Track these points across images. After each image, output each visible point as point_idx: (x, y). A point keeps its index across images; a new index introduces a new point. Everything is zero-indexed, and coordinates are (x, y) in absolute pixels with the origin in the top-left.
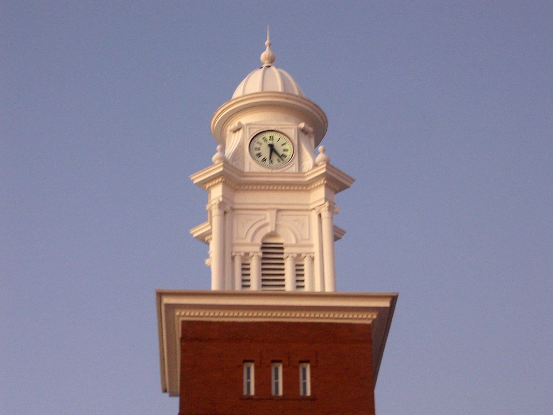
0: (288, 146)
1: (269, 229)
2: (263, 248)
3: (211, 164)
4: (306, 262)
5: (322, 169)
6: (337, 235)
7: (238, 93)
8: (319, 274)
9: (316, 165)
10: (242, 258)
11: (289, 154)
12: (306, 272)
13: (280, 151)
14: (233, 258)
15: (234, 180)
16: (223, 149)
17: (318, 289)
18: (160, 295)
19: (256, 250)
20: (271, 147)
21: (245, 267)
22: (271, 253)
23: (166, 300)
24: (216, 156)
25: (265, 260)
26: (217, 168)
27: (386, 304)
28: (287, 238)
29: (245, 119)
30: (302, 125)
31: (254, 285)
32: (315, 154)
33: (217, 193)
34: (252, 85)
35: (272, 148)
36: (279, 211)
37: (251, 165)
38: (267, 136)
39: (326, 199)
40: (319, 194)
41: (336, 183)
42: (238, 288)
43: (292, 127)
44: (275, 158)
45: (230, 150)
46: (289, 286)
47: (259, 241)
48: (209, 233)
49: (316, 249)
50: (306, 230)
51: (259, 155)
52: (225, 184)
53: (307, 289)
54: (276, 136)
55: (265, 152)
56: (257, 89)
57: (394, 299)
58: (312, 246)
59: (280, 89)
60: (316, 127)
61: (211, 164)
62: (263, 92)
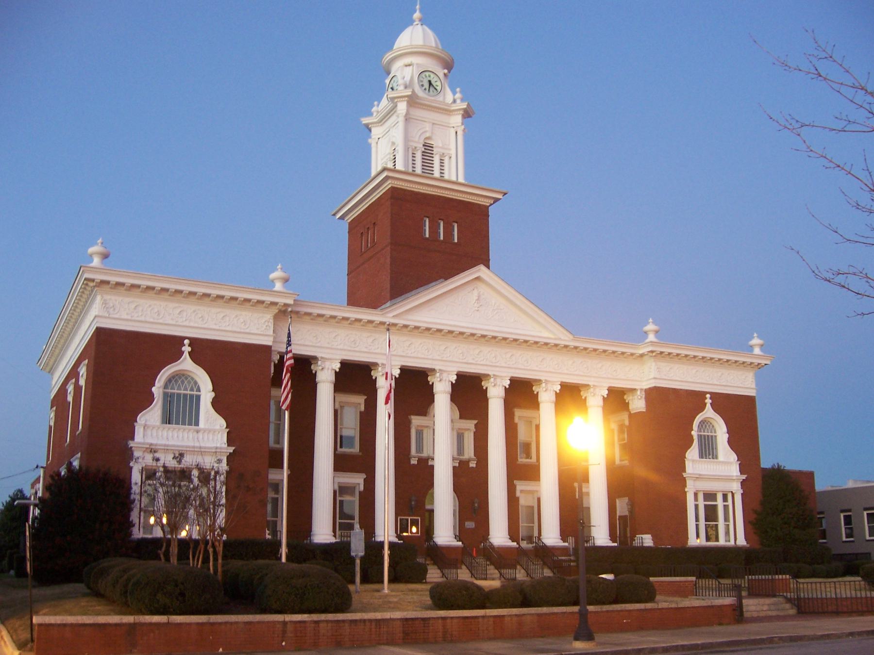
0: (439, 83)
1: (428, 135)
3: (371, 114)
4: (446, 160)
8: (452, 172)
10: (413, 150)
11: (439, 88)
13: (434, 84)
17: (454, 179)
20: (430, 81)
22: (428, 149)
28: (436, 143)
31: (419, 170)
32: (454, 93)
36: (434, 124)
37: (420, 93)
38: (427, 74)
40: (457, 120)
42: (410, 170)
46: (437, 174)
47: (422, 142)
49: (453, 152)
51: (422, 85)
52: (408, 102)
54: (432, 75)
55: (426, 85)
56: (408, 43)
58: (450, 149)
59: (434, 45)
62: (424, 46)
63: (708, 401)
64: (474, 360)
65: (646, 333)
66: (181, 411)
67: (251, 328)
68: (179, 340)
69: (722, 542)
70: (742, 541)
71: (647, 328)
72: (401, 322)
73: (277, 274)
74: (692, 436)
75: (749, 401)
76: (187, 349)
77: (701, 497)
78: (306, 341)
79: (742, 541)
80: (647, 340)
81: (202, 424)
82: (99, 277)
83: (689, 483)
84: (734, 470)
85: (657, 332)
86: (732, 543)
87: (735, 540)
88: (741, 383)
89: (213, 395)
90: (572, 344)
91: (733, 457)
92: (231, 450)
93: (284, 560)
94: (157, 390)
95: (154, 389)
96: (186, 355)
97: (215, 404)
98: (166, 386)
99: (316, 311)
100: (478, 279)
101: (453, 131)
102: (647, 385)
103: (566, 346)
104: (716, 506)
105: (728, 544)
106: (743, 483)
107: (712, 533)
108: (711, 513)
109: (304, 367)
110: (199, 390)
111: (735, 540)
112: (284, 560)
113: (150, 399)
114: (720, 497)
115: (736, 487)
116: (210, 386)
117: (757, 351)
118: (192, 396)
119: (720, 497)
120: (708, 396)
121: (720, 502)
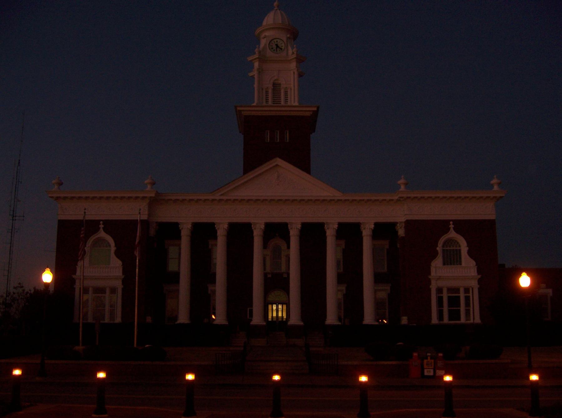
0: (283, 45)
2: (273, 85)
3: (255, 53)
4: (289, 91)
5: (295, 56)
6: (300, 75)
7: (264, 23)
8: (292, 101)
9: (293, 53)
11: (283, 48)
12: (289, 94)
14: (263, 89)
15: (263, 59)
16: (259, 47)
18: (236, 107)
19: (271, 86)
21: (267, 92)
22: (276, 86)
23: (238, 109)
24: (257, 49)
25: (274, 90)
26: (256, 56)
27: (315, 109)
29: (267, 34)
30: (288, 36)
31: (270, 103)
32: (293, 48)
33: (256, 64)
34: (269, 19)
35: (277, 45)
38: (275, 40)
39: (296, 67)
40: (293, 65)
41: (300, 60)
42: (264, 104)
43: (283, 36)
44: (278, 49)
45: (262, 46)
46: (283, 103)
48: (254, 75)
49: (292, 86)
50: (289, 78)
53: (289, 104)
54: (279, 41)
55: (275, 47)
57: (318, 108)
60: (294, 35)
61: (255, 53)
63: (452, 226)
64: (277, 215)
65: (399, 185)
66: (452, 258)
67: (133, 211)
68: (447, 222)
69: (463, 320)
70: (478, 320)
71: (492, 182)
72: (224, 198)
73: (401, 181)
74: (437, 251)
75: (492, 223)
76: (102, 226)
77: (445, 291)
78: (167, 214)
79: (478, 320)
80: (401, 190)
81: (463, 264)
82: (405, 196)
83: (433, 282)
84: (473, 272)
85: (499, 184)
86: (472, 321)
87: (474, 319)
88: (483, 211)
89: (467, 248)
90: (343, 198)
91: (473, 263)
92: (479, 277)
93: (135, 346)
94: (439, 249)
95: (438, 249)
96: (452, 229)
97: (469, 253)
98: (443, 246)
99: (174, 198)
100: (277, 165)
101: (292, 72)
102: (403, 219)
103: (338, 200)
104: (459, 297)
105: (469, 322)
106: (479, 281)
107: (454, 315)
108: (454, 302)
109: (171, 231)
110: (460, 246)
111: (474, 319)
112: (135, 346)
113: (437, 253)
114: (462, 290)
115: (474, 284)
116: (465, 244)
117: (496, 188)
118: (456, 250)
119: (462, 290)
120: (451, 223)
121: (462, 295)
